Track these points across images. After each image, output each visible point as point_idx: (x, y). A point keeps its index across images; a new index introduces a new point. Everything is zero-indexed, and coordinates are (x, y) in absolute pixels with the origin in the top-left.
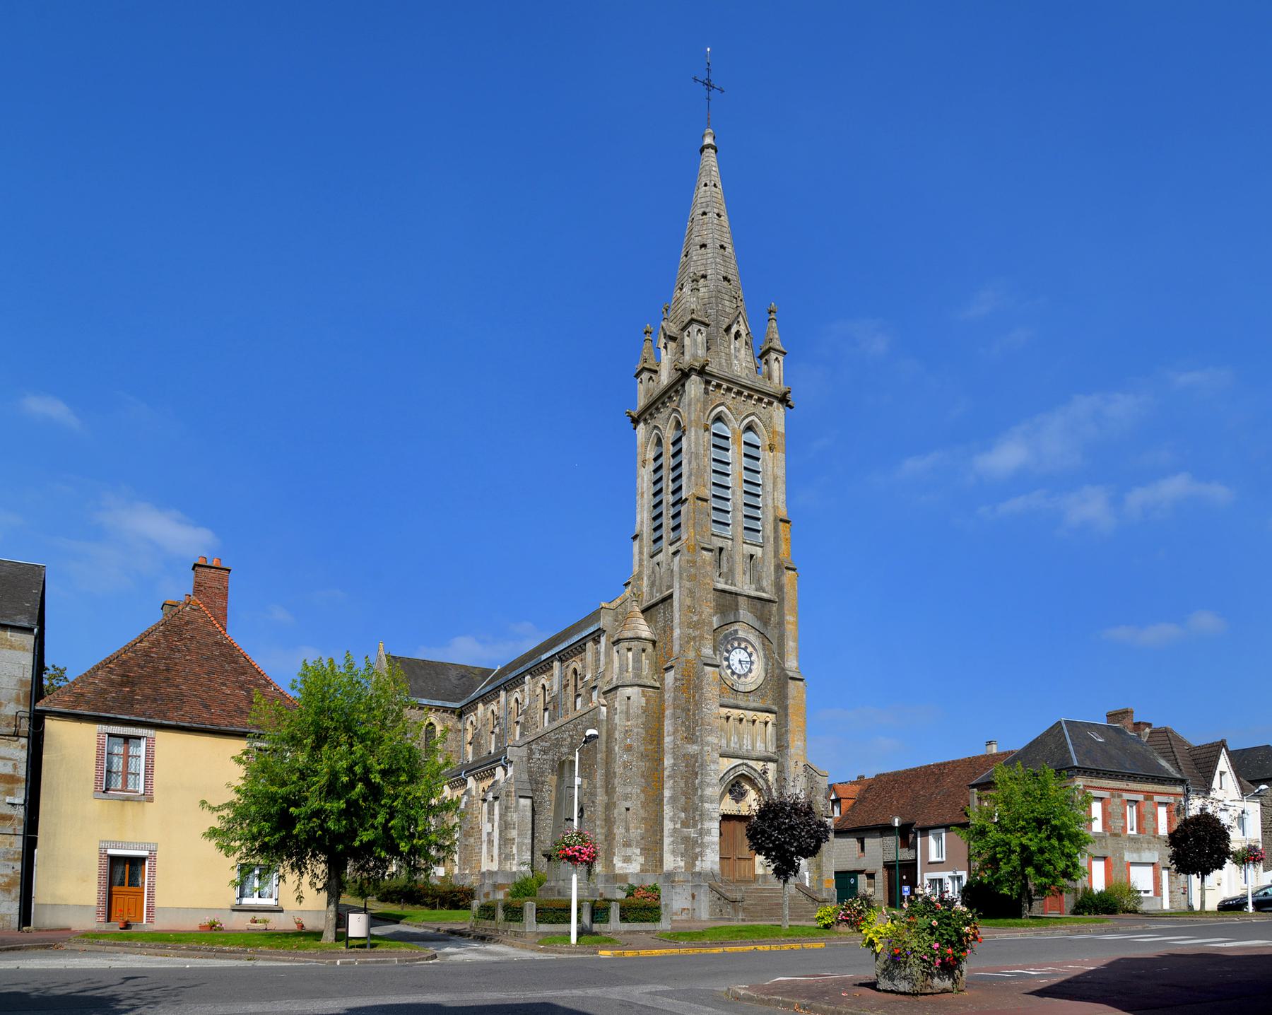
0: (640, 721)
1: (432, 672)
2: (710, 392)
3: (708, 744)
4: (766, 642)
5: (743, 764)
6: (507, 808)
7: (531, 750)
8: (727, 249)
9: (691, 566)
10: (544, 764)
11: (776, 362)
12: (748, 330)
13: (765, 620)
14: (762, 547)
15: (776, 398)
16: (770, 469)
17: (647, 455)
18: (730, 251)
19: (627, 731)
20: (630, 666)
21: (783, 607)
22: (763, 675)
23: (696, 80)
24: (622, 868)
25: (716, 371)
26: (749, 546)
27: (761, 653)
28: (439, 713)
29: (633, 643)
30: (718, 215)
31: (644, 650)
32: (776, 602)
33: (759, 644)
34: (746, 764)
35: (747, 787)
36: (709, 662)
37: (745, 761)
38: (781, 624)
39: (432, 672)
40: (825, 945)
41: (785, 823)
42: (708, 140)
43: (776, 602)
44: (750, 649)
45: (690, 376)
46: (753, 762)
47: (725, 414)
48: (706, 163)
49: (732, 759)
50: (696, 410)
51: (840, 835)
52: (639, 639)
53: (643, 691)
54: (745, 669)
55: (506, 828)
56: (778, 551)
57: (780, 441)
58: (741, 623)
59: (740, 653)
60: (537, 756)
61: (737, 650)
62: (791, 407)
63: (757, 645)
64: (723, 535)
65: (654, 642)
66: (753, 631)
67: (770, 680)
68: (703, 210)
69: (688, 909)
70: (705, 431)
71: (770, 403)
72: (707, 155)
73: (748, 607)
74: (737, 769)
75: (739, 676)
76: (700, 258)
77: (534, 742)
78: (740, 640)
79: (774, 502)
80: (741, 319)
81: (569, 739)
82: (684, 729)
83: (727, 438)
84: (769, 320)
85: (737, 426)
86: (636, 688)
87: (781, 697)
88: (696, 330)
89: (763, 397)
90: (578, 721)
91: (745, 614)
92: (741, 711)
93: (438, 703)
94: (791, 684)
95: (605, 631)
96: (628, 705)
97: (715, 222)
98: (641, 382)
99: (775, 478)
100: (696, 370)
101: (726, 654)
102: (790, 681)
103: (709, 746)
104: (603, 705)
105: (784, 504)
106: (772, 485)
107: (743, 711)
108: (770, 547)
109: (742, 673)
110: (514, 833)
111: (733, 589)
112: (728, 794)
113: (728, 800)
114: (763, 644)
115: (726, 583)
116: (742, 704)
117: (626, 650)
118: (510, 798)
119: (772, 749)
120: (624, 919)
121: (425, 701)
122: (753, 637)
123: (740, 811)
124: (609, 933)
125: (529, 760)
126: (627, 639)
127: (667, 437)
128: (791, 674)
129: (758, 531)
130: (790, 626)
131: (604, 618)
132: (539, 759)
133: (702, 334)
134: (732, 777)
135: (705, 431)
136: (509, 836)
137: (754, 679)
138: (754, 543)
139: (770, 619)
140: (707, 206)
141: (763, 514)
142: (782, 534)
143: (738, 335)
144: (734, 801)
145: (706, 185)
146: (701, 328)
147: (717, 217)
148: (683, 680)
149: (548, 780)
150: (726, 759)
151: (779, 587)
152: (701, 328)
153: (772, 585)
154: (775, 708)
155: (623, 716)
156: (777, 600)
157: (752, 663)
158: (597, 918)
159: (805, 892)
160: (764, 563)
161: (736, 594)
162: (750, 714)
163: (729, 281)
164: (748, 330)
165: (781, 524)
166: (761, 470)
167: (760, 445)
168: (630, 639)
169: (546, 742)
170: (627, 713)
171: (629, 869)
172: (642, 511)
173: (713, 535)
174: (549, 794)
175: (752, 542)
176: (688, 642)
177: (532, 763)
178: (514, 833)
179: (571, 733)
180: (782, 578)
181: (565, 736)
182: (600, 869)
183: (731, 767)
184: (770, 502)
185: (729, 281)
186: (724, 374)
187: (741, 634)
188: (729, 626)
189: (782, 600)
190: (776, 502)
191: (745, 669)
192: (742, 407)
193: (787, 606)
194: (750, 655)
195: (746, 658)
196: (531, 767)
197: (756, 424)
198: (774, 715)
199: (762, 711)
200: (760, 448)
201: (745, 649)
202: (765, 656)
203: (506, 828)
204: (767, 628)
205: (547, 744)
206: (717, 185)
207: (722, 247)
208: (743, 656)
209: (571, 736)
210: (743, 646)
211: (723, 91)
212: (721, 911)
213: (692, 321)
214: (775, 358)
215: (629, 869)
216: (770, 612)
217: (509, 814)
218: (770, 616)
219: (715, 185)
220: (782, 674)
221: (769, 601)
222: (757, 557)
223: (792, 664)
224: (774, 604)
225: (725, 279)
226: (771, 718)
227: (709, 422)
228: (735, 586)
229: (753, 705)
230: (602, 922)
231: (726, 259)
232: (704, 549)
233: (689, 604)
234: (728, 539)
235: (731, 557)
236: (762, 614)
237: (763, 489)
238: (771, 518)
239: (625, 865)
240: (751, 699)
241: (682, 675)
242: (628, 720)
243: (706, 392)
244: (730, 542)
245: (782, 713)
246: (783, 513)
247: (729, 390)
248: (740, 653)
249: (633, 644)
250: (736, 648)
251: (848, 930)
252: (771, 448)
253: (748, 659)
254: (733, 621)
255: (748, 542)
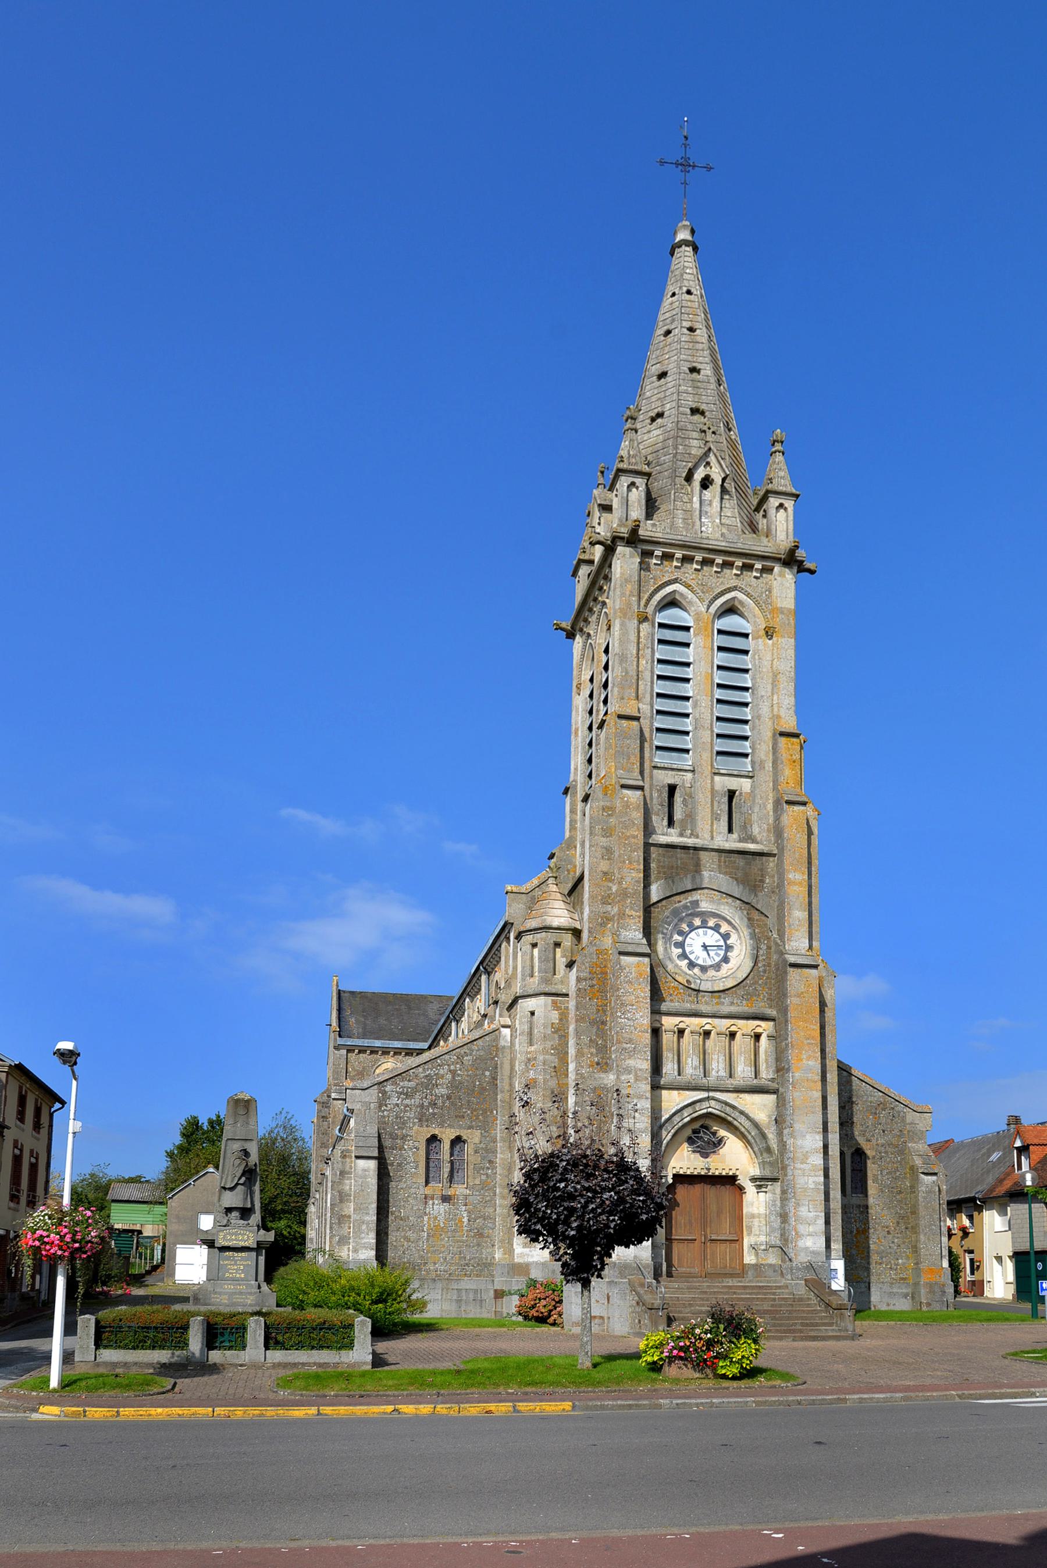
0: (549, 1044)
1: (403, 1007)
2: (652, 567)
3: (628, 1070)
4: (756, 916)
5: (708, 1098)
6: (343, 1173)
7: (384, 1093)
8: (702, 372)
9: (609, 815)
10: (406, 1111)
11: (782, 511)
12: (724, 471)
13: (753, 884)
14: (751, 777)
15: (777, 560)
16: (766, 663)
17: (583, 676)
18: (709, 373)
19: (529, 1060)
20: (536, 969)
21: (782, 861)
22: (748, 965)
23: (662, 163)
24: (522, 1255)
25: (660, 535)
26: (727, 778)
27: (745, 932)
28: (400, 1057)
29: (538, 935)
30: (691, 329)
31: (557, 945)
32: (774, 855)
33: (741, 919)
34: (714, 1099)
35: (722, 1133)
36: (630, 949)
37: (711, 1094)
38: (780, 887)
39: (403, 1007)
40: (574, 1407)
41: (558, 1189)
42: (683, 235)
43: (774, 855)
44: (725, 928)
45: (616, 549)
46: (729, 1094)
47: (682, 595)
48: (676, 267)
49: (687, 1092)
50: (623, 594)
51: (1016, 1199)
52: (547, 928)
53: (554, 1003)
54: (715, 957)
55: (341, 1201)
56: (777, 780)
57: (786, 624)
58: (706, 891)
59: (698, 935)
60: (395, 1100)
61: (700, 931)
62: (812, 572)
63: (737, 921)
64: (675, 766)
65: (577, 933)
66: (730, 900)
67: (765, 971)
68: (666, 328)
69: (602, 1318)
70: (640, 622)
71: (769, 570)
72: (679, 255)
73: (720, 866)
74: (697, 1106)
75: (704, 969)
76: (655, 393)
77: (390, 1082)
78: (704, 916)
79: (773, 710)
80: (712, 458)
81: (449, 1076)
82: (594, 1050)
83: (687, 629)
84: (771, 455)
85: (703, 609)
86: (542, 998)
87: (779, 997)
88: (626, 484)
89: (754, 562)
90: (465, 1049)
91: (711, 874)
92: (704, 1021)
93: (398, 1044)
94: (793, 974)
95: (512, 924)
96: (531, 1023)
97: (683, 339)
98: (579, 581)
99: (775, 675)
100: (622, 538)
101: (677, 938)
102: (791, 970)
103: (630, 1073)
104: (504, 1026)
105: (792, 712)
106: (769, 687)
107: (709, 1020)
108: (765, 778)
109: (709, 962)
110: (350, 1208)
111: (690, 841)
112: (686, 1145)
113: (686, 1153)
114: (749, 919)
115: (681, 835)
116: (704, 1008)
117: (529, 947)
118: (348, 1160)
119: (766, 1074)
120: (270, 1342)
121: (378, 1043)
122: (727, 909)
123: (708, 1169)
124: (241, 1365)
125: (380, 1107)
126: (531, 930)
127: (599, 644)
128: (792, 959)
129: (746, 755)
130: (796, 888)
131: (510, 906)
132: (397, 1105)
133: (637, 488)
134: (688, 1119)
135: (640, 622)
136: (346, 1212)
137: (733, 970)
138: (735, 773)
139: (762, 881)
140: (673, 321)
141: (752, 730)
142: (784, 755)
143: (706, 483)
144: (698, 1155)
145: (674, 295)
146: (635, 480)
147: (688, 332)
148: (591, 979)
149: (412, 1133)
150: (675, 1092)
151: (778, 831)
152: (635, 480)
153: (769, 831)
154: (773, 1012)
155: (525, 1038)
156: (775, 852)
157: (729, 948)
158: (222, 1342)
159: (816, 1291)
160: (754, 801)
161: (695, 849)
162: (724, 1024)
163: (703, 413)
164: (724, 471)
165: (783, 740)
166: (750, 667)
167: (750, 631)
168: (535, 930)
169: (409, 1081)
170: (530, 1033)
171: (532, 1256)
172: (576, 755)
173: (655, 767)
174: (414, 1153)
175: (730, 772)
176: (603, 925)
177: (385, 1110)
178: (350, 1208)
179: (452, 1067)
180: (782, 818)
181: (442, 1072)
182: (501, 1256)
183: (686, 1103)
184: (765, 710)
185: (703, 413)
186: (675, 537)
187: (705, 906)
188: (682, 896)
189: (781, 849)
190: (776, 710)
191: (715, 957)
192: (713, 581)
193: (788, 860)
194: (726, 937)
195: (719, 940)
196: (384, 1117)
197: (741, 602)
198: (772, 1023)
199: (747, 1018)
200: (750, 637)
201: (716, 928)
202: (753, 936)
203: (341, 1201)
204: (756, 895)
205: (412, 1084)
206: (693, 290)
207: (693, 370)
208: (712, 938)
209: (454, 1073)
210: (711, 923)
211: (711, 168)
212: (640, 1322)
213: (620, 471)
214: (777, 504)
215: (532, 1256)
216: (762, 870)
217: (347, 1182)
218: (762, 876)
219: (689, 292)
220: (781, 959)
221: (761, 854)
222: (741, 794)
223: (797, 944)
224: (771, 859)
225: (695, 411)
226: (765, 1028)
227: (650, 609)
228: (697, 837)
229: (726, 1009)
230: (230, 1348)
231: (699, 384)
232: (623, 786)
233: (605, 869)
234: (686, 771)
235: (690, 796)
236: (746, 875)
237: (753, 693)
238: (767, 734)
239: (527, 1250)
240: (727, 1001)
241: (590, 973)
242: (531, 1044)
243: (644, 567)
244: (690, 775)
245: (782, 1019)
246: (790, 723)
247: (687, 559)
248: (698, 935)
249: (538, 937)
250: (698, 928)
251: (689, 1372)
252: (769, 633)
253: (722, 943)
254: (689, 888)
255: (722, 771)
